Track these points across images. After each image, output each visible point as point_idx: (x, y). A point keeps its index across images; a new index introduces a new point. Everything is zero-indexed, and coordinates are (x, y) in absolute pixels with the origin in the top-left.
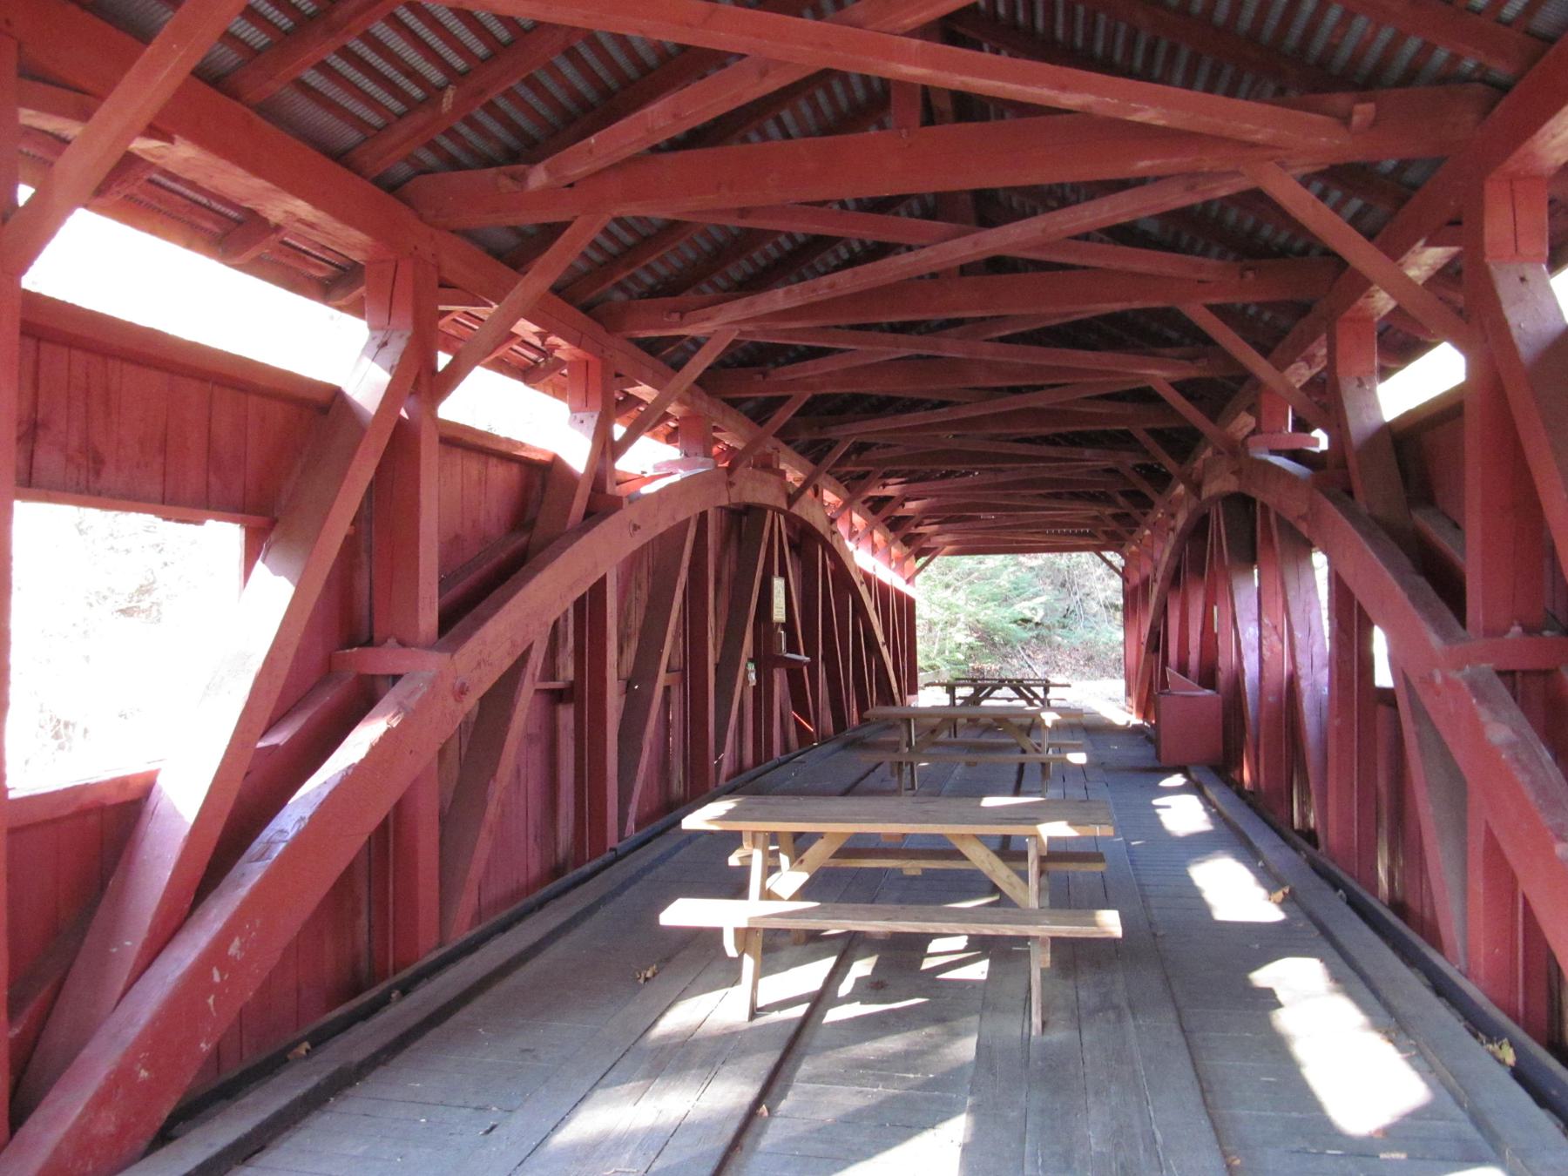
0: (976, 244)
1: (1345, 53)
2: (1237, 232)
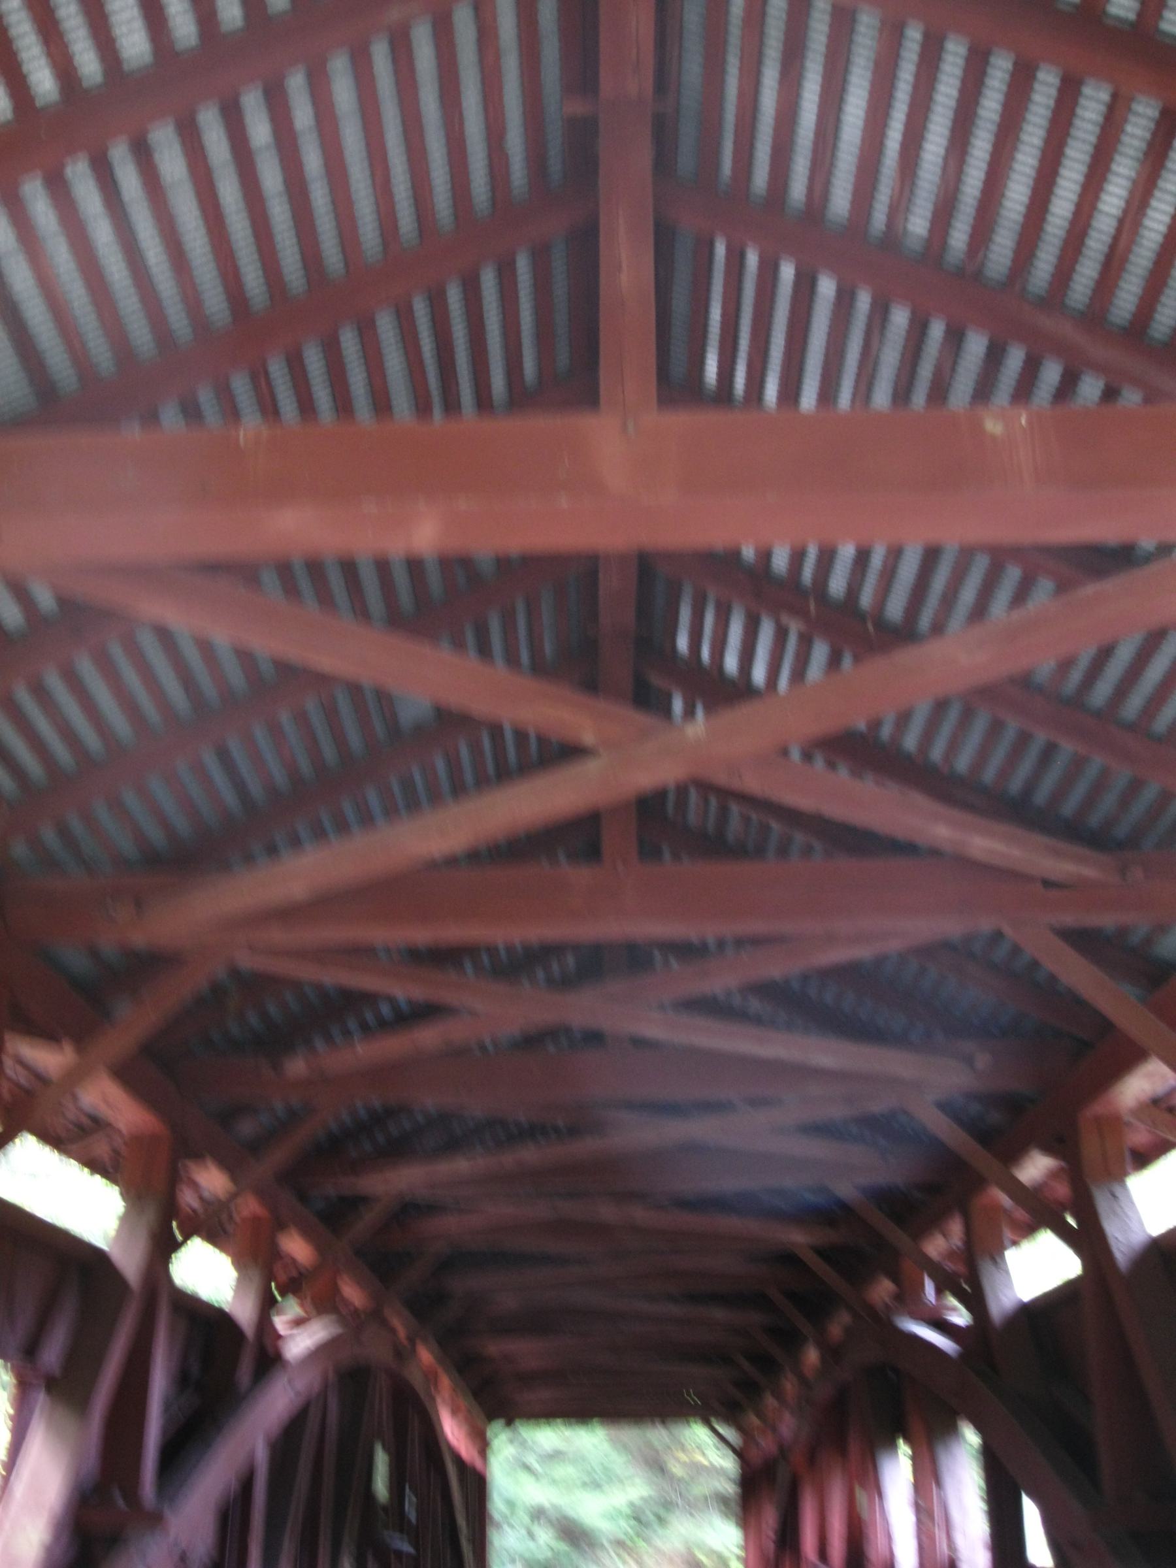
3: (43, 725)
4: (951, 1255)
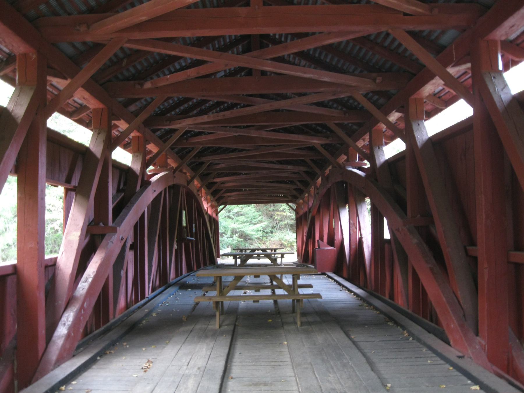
0: (271, 106)
1: (374, 61)
2: (348, 106)
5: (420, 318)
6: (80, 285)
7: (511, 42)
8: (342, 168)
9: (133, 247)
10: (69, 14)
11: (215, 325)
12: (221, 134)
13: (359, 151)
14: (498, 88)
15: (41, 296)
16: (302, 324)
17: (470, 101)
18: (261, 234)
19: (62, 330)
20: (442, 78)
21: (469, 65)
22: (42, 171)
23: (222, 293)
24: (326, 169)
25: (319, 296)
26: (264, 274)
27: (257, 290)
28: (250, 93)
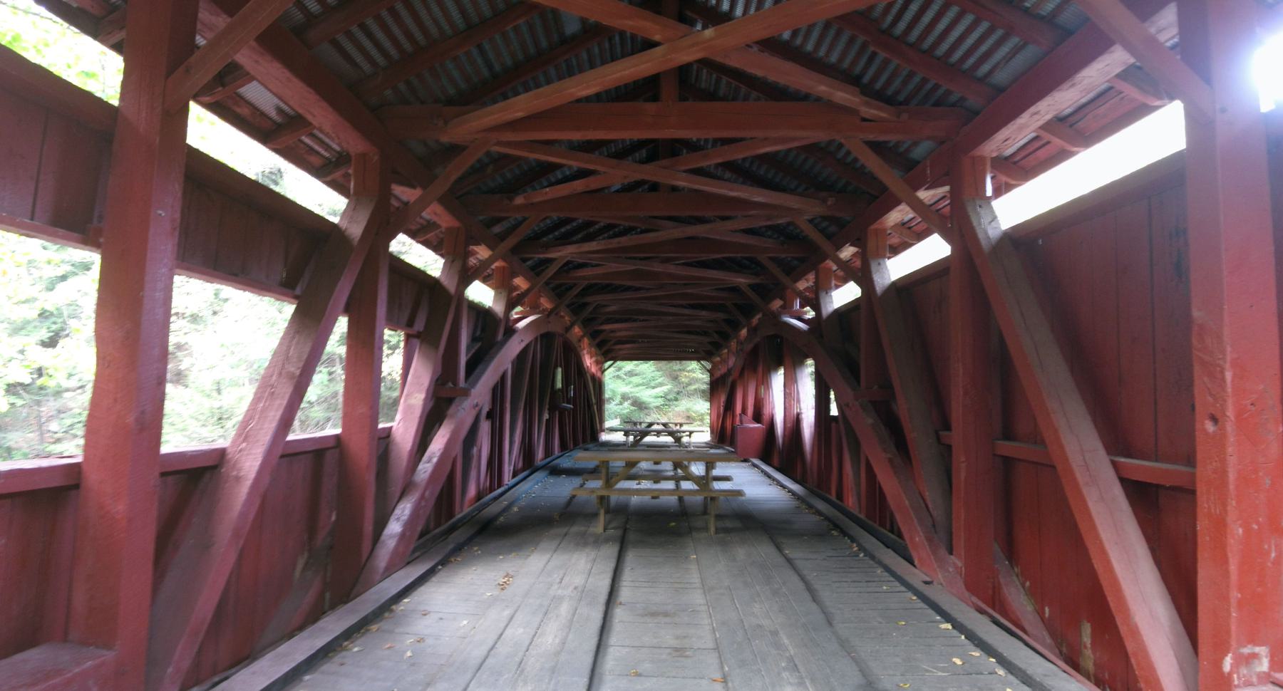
2: (787, 234)
3: (396, 30)
4: (807, 289)
5: (876, 526)
6: (420, 467)
7: (1006, 158)
8: (774, 318)
9: (490, 415)
10: (423, 103)
11: (598, 527)
12: (613, 267)
13: (799, 294)
14: (985, 220)
15: (371, 478)
16: (717, 531)
17: (947, 236)
18: (660, 402)
19: (394, 527)
20: (908, 204)
21: (947, 188)
22: (381, 310)
23: (609, 483)
24: (753, 316)
25: (739, 493)
26: (667, 460)
27: (656, 482)
28: (656, 214)
